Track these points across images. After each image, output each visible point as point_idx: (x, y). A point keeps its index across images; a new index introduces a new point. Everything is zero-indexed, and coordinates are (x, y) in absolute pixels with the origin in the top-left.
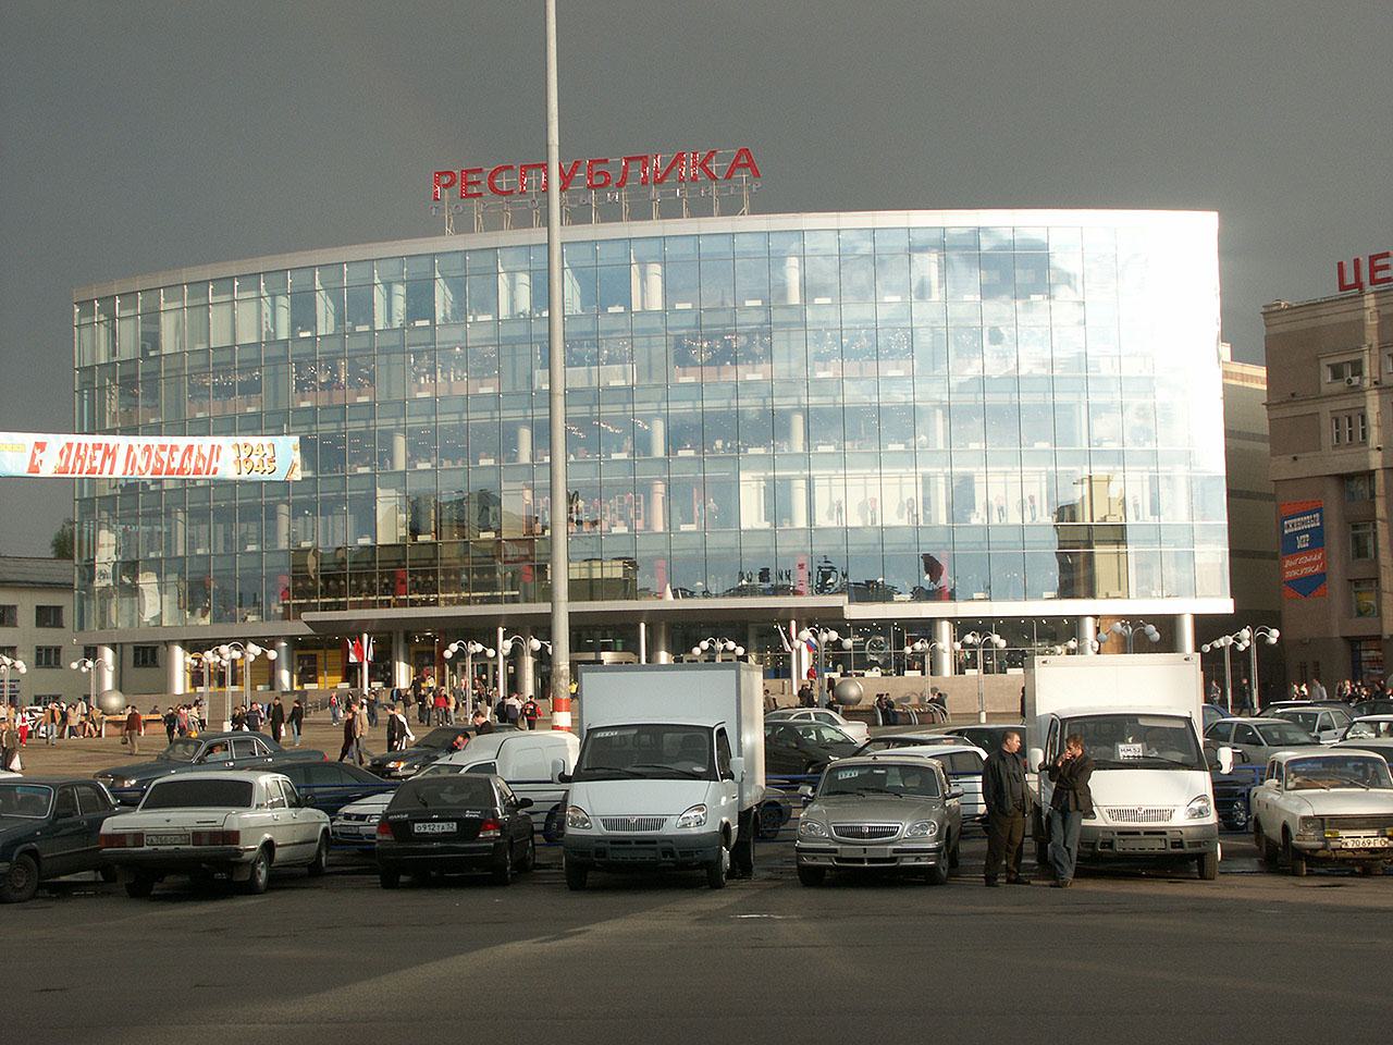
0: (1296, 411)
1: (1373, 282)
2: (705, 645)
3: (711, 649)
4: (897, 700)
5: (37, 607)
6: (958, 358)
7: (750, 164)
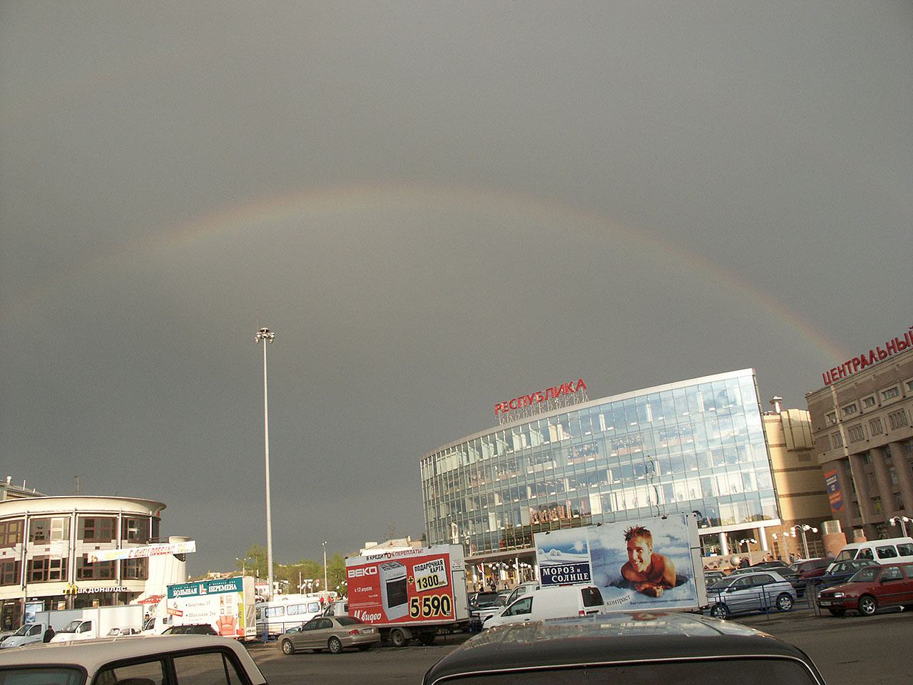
0: (820, 435)
1: (834, 380)
2: (743, 541)
3: (745, 544)
4: (498, 591)
5: (448, 554)
6: (661, 440)
7: (583, 385)
